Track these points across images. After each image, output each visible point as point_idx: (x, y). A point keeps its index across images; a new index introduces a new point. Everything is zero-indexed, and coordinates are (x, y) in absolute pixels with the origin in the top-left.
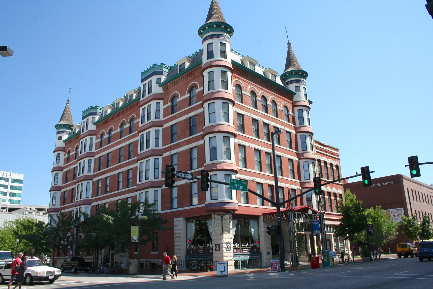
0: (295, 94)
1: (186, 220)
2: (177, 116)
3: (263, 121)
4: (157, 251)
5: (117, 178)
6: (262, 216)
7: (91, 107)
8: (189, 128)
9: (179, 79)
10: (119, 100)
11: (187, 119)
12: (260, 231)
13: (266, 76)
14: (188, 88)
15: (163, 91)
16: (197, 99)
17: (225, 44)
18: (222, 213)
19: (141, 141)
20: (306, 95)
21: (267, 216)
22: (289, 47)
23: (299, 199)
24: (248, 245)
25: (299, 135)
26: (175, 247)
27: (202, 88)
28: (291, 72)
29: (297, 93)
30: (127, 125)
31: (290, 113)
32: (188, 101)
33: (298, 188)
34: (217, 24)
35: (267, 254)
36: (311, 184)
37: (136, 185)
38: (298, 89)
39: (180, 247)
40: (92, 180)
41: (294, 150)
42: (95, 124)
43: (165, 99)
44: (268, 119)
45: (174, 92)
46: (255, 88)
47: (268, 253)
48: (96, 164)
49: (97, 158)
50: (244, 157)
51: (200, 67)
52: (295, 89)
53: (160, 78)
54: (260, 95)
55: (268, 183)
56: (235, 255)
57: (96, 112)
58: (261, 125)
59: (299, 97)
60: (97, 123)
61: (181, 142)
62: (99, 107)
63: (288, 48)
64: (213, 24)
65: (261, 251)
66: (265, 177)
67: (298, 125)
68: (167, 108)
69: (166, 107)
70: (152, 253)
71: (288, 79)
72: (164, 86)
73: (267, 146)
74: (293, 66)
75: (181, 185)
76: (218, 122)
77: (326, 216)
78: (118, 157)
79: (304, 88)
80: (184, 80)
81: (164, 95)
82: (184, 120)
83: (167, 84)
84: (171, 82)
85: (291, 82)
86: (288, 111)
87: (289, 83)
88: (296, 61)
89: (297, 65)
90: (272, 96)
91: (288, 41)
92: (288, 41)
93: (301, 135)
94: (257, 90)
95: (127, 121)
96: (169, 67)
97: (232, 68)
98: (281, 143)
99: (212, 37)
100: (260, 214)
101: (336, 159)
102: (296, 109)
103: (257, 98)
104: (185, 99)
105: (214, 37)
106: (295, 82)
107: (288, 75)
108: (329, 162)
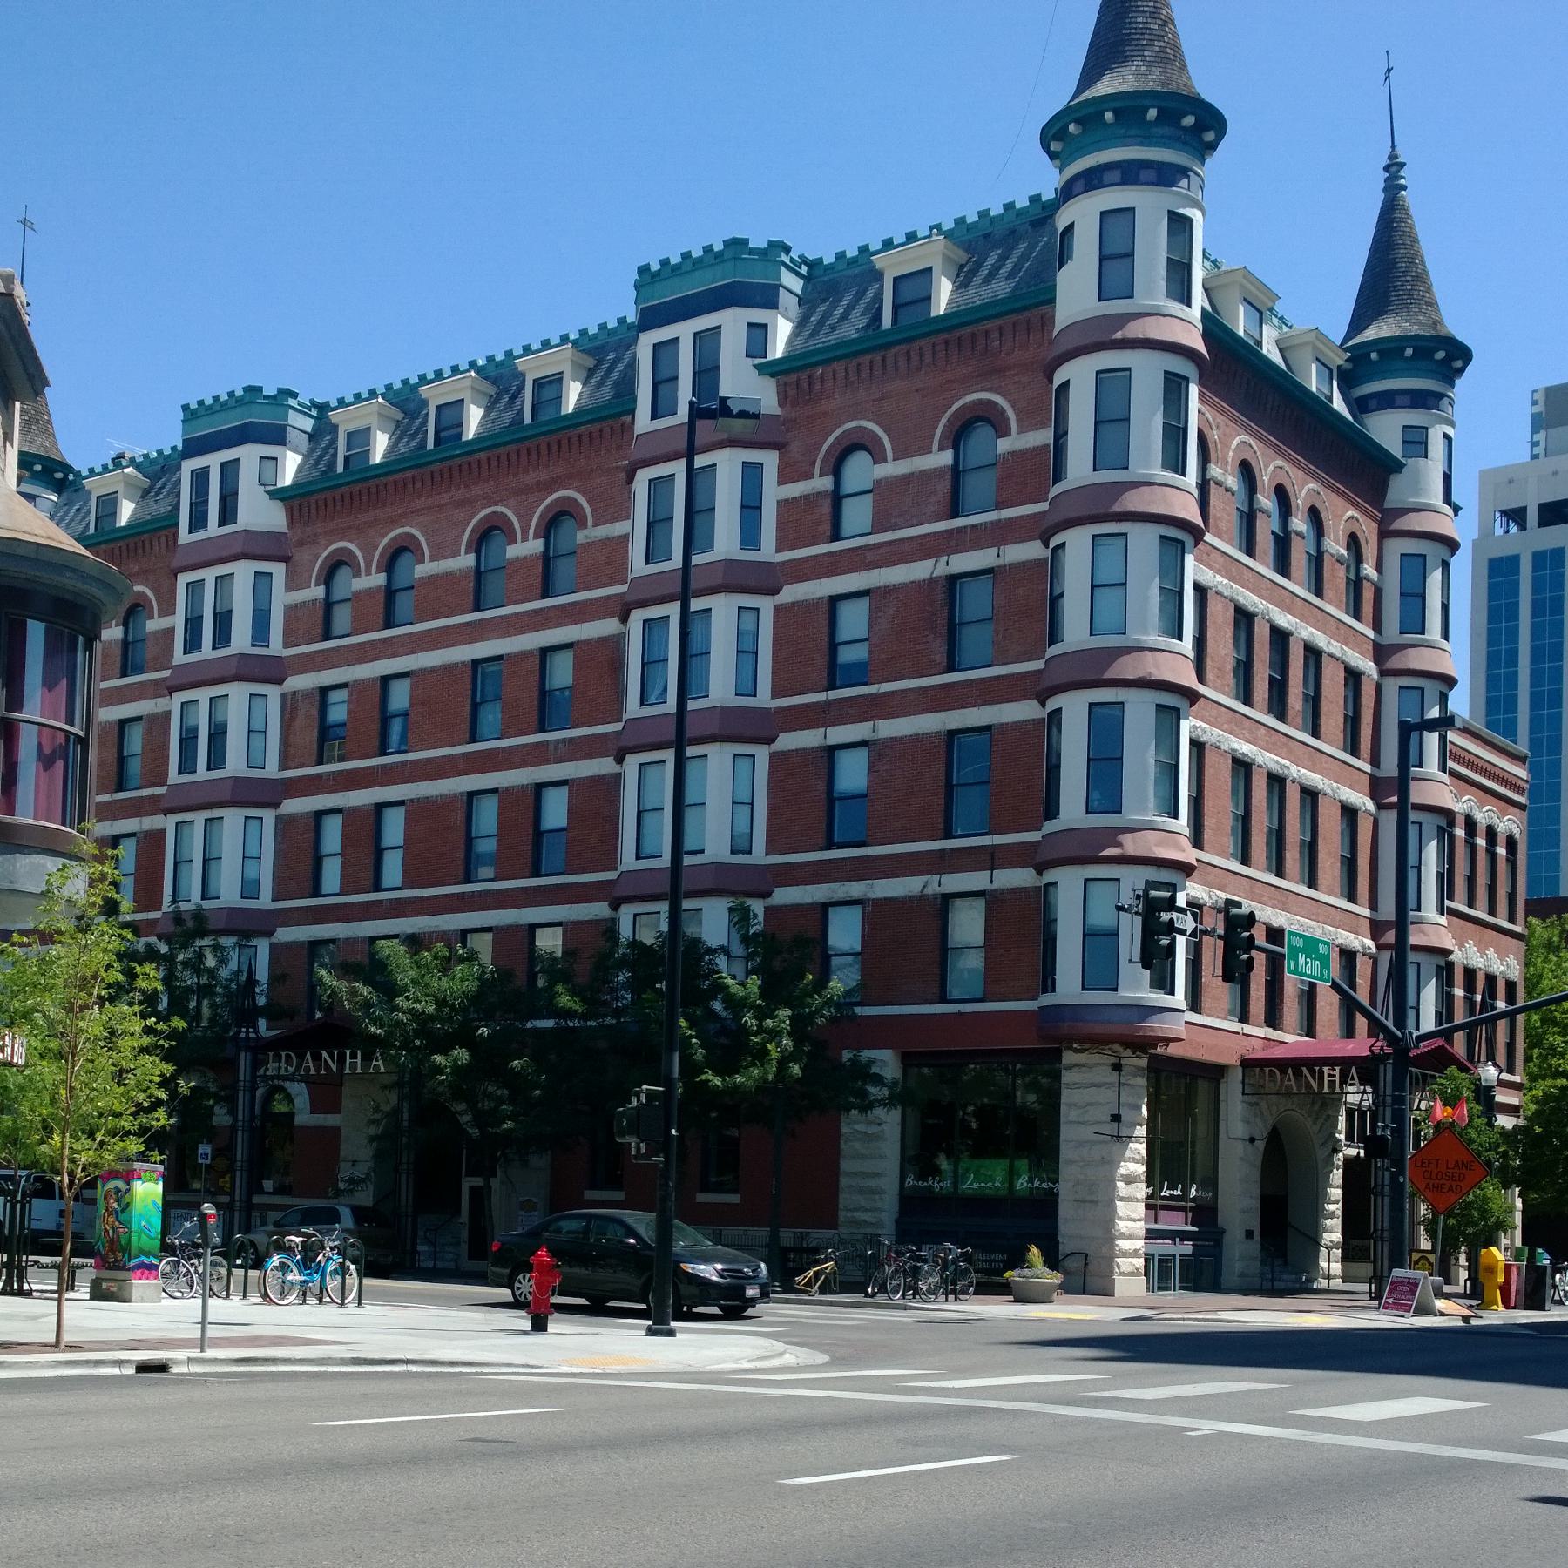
0: (1398, 467)
1: (902, 1063)
2: (870, 556)
3: (1269, 621)
4: (735, 1191)
5: (460, 816)
6: (1240, 1070)
7: (253, 390)
8: (944, 630)
9: (889, 362)
10: (460, 390)
11: (932, 581)
12: (1222, 1134)
13: (1219, 315)
14: (943, 421)
15: (781, 404)
16: (999, 488)
17: (1188, 222)
18: (1116, 1047)
19: (646, 656)
20: (1447, 479)
21: (1267, 1070)
22: (1393, 188)
23: (1502, 1026)
24: (1179, 1192)
25: (1392, 686)
26: (844, 1181)
27: (1045, 436)
28: (1392, 345)
29: (1411, 461)
30: (530, 547)
31: (1369, 570)
32: (945, 486)
33: (1363, 947)
34: (1164, 104)
35: (1244, 1235)
36: (1423, 932)
37: (160, 780)
38: (1416, 441)
39: (873, 1183)
40: (276, 806)
41: (1363, 760)
42: (277, 494)
43: (795, 449)
44: (1289, 610)
45: (853, 424)
46: (1256, 448)
47: (1249, 1234)
48: (300, 722)
49: (307, 694)
50: (1244, 818)
51: (1028, 321)
52: (1404, 442)
53: (765, 326)
54: (1269, 480)
55: (1267, 920)
56: (1150, 1235)
57: (285, 426)
58: (1262, 634)
59: (1417, 487)
60: (291, 498)
61: (893, 693)
62: (295, 395)
63: (1385, 190)
64: (1147, 102)
65: (1221, 1220)
66: (1338, 915)
67: (1392, 633)
68: (809, 500)
69: (796, 494)
70: (701, 1198)
71: (1370, 379)
72: (793, 377)
73: (1274, 744)
74: (1407, 307)
75: (886, 899)
76: (1135, 636)
77: (1501, 1094)
78: (468, 709)
79: (1446, 436)
80: (919, 369)
81: (786, 423)
82: (916, 584)
83: (808, 371)
84: (839, 367)
85: (1387, 401)
86: (1359, 559)
87: (1373, 403)
88: (1422, 278)
89: (1428, 303)
90: (1311, 486)
91: (1393, 147)
92: (1393, 147)
93: (1400, 687)
94: (1263, 454)
95: (525, 520)
96: (804, 261)
97: (1205, 352)
98: (1323, 729)
99: (1130, 173)
100: (1232, 1060)
101: (1512, 809)
102: (1396, 547)
103: (1212, 466)
104: (923, 473)
105: (1144, 175)
106: (1406, 399)
107: (1374, 356)
108: (1483, 821)
